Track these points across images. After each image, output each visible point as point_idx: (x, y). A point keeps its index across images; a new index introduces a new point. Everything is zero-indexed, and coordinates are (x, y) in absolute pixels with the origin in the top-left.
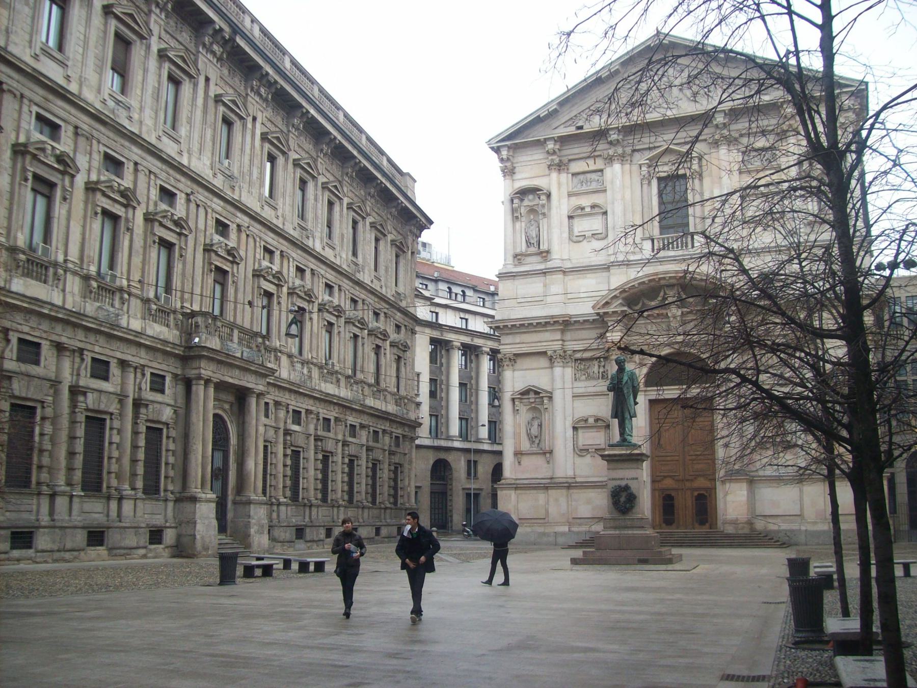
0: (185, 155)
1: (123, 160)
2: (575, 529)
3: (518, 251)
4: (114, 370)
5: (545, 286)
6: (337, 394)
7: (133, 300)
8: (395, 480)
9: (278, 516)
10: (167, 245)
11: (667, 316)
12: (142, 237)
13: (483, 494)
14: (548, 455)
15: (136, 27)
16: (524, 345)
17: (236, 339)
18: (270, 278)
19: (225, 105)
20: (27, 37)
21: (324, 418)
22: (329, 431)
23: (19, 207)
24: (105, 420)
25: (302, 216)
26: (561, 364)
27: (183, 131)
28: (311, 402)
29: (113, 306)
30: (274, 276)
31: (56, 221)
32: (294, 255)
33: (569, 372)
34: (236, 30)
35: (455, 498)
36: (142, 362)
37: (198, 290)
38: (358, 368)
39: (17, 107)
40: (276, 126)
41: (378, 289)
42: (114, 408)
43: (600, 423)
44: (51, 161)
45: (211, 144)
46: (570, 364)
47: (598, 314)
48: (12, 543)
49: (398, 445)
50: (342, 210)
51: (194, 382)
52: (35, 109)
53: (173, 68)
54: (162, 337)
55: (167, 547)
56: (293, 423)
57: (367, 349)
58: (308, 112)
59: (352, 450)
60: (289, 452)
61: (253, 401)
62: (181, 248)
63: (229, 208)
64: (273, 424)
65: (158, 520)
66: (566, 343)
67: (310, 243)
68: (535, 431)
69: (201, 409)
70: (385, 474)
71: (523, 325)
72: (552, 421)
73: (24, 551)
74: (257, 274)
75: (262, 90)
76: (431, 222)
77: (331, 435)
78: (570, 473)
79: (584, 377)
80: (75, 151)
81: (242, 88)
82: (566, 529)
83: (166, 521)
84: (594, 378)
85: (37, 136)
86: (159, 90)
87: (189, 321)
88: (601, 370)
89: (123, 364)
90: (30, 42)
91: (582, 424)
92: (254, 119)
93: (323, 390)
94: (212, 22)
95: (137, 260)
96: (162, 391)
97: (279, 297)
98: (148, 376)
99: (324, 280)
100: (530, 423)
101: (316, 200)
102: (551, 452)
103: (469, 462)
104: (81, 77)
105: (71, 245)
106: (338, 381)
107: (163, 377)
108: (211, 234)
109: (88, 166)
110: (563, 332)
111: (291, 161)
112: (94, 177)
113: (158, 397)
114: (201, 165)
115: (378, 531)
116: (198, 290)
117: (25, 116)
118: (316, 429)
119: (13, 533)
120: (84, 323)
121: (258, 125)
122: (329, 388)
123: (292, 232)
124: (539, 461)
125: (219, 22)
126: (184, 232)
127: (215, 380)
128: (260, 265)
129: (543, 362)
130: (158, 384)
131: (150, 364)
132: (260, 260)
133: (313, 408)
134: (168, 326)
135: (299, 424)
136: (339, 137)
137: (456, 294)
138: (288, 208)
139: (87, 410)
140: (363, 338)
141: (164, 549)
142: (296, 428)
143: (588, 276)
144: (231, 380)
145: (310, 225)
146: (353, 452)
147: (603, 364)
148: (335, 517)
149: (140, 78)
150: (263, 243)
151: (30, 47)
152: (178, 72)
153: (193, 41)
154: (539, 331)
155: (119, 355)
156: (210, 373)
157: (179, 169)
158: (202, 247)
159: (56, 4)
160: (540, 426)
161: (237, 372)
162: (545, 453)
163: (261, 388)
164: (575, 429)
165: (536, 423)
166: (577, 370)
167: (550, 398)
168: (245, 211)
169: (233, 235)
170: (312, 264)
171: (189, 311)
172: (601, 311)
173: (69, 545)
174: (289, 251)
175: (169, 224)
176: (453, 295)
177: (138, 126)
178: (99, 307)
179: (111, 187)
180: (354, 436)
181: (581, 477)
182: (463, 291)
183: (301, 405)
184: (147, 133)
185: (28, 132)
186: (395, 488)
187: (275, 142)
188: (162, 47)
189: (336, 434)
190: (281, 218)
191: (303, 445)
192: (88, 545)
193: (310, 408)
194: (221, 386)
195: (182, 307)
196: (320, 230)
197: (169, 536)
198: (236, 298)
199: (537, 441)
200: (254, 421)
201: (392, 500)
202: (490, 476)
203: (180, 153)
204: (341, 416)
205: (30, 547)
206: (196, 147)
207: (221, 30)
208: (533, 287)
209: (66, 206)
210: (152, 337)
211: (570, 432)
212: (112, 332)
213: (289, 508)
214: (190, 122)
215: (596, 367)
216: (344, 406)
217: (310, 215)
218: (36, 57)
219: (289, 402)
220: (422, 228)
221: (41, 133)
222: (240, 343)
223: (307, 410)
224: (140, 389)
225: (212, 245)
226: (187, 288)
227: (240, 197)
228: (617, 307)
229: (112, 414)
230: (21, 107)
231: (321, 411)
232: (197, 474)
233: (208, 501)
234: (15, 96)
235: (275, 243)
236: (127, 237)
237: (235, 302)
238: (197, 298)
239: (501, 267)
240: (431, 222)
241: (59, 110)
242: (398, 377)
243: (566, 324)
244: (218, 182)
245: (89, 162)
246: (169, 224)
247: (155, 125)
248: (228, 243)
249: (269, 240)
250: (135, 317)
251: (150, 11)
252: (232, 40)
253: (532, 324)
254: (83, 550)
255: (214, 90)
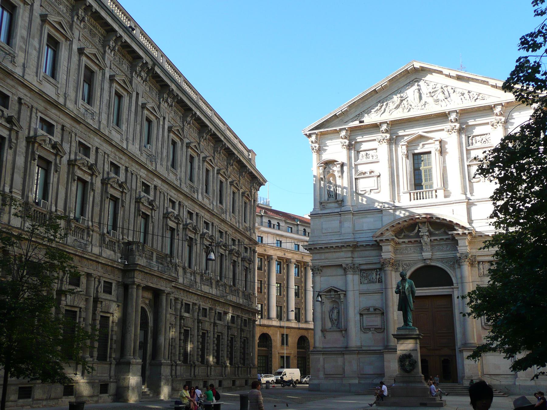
0: (125, 142)
1: (90, 146)
2: (362, 382)
3: (323, 200)
4: (83, 280)
5: (340, 222)
6: (211, 292)
7: (95, 234)
8: (244, 348)
9: (176, 373)
10: (115, 200)
11: (420, 242)
12: (100, 195)
13: (292, 356)
14: (344, 332)
15: (97, 62)
16: (327, 260)
17: (154, 259)
18: (173, 219)
19: (148, 110)
20: (35, 70)
21: (203, 308)
22: (206, 317)
23: (29, 176)
24: (109, 317)
25: (191, 179)
26: (352, 273)
27: (124, 127)
28: (196, 298)
29: (83, 238)
30: (175, 218)
31: (51, 185)
32: (186, 204)
33: (357, 277)
34: (155, 63)
35: (273, 360)
36: (99, 274)
37: (131, 228)
38: (223, 275)
39: (29, 114)
40: (176, 123)
41: (234, 224)
42: (82, 305)
43: (377, 312)
44: (48, 147)
45: (139, 135)
46: (357, 273)
47: (376, 241)
48: (19, 394)
49: (245, 326)
50: (213, 175)
51: (130, 286)
52: (39, 114)
53: (118, 87)
54: (111, 258)
55: (110, 395)
56: (185, 312)
57: (227, 264)
58: (196, 113)
59: (219, 329)
60: (183, 331)
61: (164, 298)
62: (122, 201)
63: (150, 175)
64: (174, 313)
65: (105, 377)
66: (354, 259)
67: (195, 196)
68: (335, 316)
69: (134, 304)
70: (238, 344)
71: (327, 248)
72: (346, 309)
73: (25, 400)
74: (166, 216)
75: (169, 100)
76: (265, 181)
77: (207, 319)
78: (359, 344)
79: (366, 281)
80: (62, 141)
81: (157, 99)
82: (356, 381)
83: (110, 378)
84: (373, 282)
85: (40, 132)
86: (110, 101)
87: (128, 250)
88: (378, 277)
89: (89, 275)
90: (37, 73)
91: (366, 312)
92: (164, 118)
93: (203, 290)
94: (140, 58)
95: (97, 209)
96: (110, 293)
97: (178, 231)
98: (102, 283)
99: (204, 219)
100: (332, 310)
101: (199, 168)
102: (346, 330)
103: (283, 335)
104: (65, 94)
105: (59, 200)
106: (211, 284)
107: (111, 284)
108: (140, 192)
109: (70, 149)
110: (352, 252)
111: (185, 145)
112: (73, 157)
113: (108, 296)
114: (134, 149)
115: (234, 382)
116: (131, 228)
117: (34, 120)
118: (198, 316)
119: (20, 388)
120: (67, 250)
121: (166, 122)
122: (206, 289)
123: (185, 189)
124: (337, 336)
125: (146, 58)
126: (125, 191)
127: (143, 285)
128: (167, 210)
129: (340, 271)
130: (108, 289)
131: (104, 275)
132: (167, 207)
133: (197, 302)
134: (114, 251)
135: (188, 313)
136: (213, 129)
137: (274, 225)
138: (183, 174)
139: (67, 305)
140: (226, 256)
141: (109, 396)
142: (186, 315)
143: (368, 216)
144: (151, 285)
145: (195, 185)
146: (219, 330)
147: (379, 273)
148: (209, 374)
149: (99, 94)
150: (169, 197)
151: (37, 76)
152: (121, 89)
153: (129, 70)
154: (337, 252)
155: (86, 270)
156: (140, 281)
157: (122, 151)
158: (134, 200)
159: (51, 48)
160: (338, 313)
161: (155, 279)
162: (341, 331)
163: (169, 289)
164: (361, 315)
165: (335, 311)
166: (361, 276)
167: (345, 295)
168: (159, 177)
169: (152, 192)
170: (197, 209)
171: (126, 241)
172: (378, 239)
173: (53, 395)
174: (184, 202)
175: (116, 186)
176: (307, 233)
177: (98, 125)
178: (75, 239)
179: (83, 164)
180: (220, 320)
181: (365, 346)
182: (278, 223)
183: (190, 300)
184: (104, 129)
185: (36, 130)
186: (244, 354)
187: (176, 133)
188: (112, 74)
189: (210, 319)
190: (179, 181)
191: (191, 326)
192: (64, 395)
193: (195, 302)
194: (146, 288)
195: (123, 239)
196: (201, 187)
197: (112, 388)
198: (153, 232)
199: (336, 323)
200: (164, 311)
201: (242, 361)
202: (296, 345)
203: (122, 141)
204: (213, 307)
205: (30, 397)
206: (131, 138)
207: (147, 63)
208: (333, 224)
209: (56, 175)
210: (106, 258)
211: (358, 316)
212: (83, 255)
213: (182, 368)
214: (128, 121)
215: (374, 275)
216: (215, 301)
217: (195, 179)
218: (40, 82)
219: (183, 298)
220: (261, 184)
221: (42, 130)
222: (157, 262)
223: (193, 303)
224: (97, 291)
225: (141, 199)
226: (126, 226)
227: (156, 168)
228: (389, 235)
229: (81, 308)
230: (31, 114)
231: (201, 303)
232: (130, 347)
233: (137, 364)
234: (28, 107)
235: (176, 196)
236: (92, 193)
237: (153, 235)
238: (131, 232)
239: (312, 210)
240: (265, 181)
241: (53, 116)
242: (246, 281)
243: (355, 247)
244: (143, 159)
245: (70, 148)
246: (116, 186)
247: (108, 124)
248: (148, 197)
249: (173, 195)
250: (96, 246)
251: (105, 52)
252: (153, 69)
253: (332, 247)
254: (61, 398)
255: (141, 101)
